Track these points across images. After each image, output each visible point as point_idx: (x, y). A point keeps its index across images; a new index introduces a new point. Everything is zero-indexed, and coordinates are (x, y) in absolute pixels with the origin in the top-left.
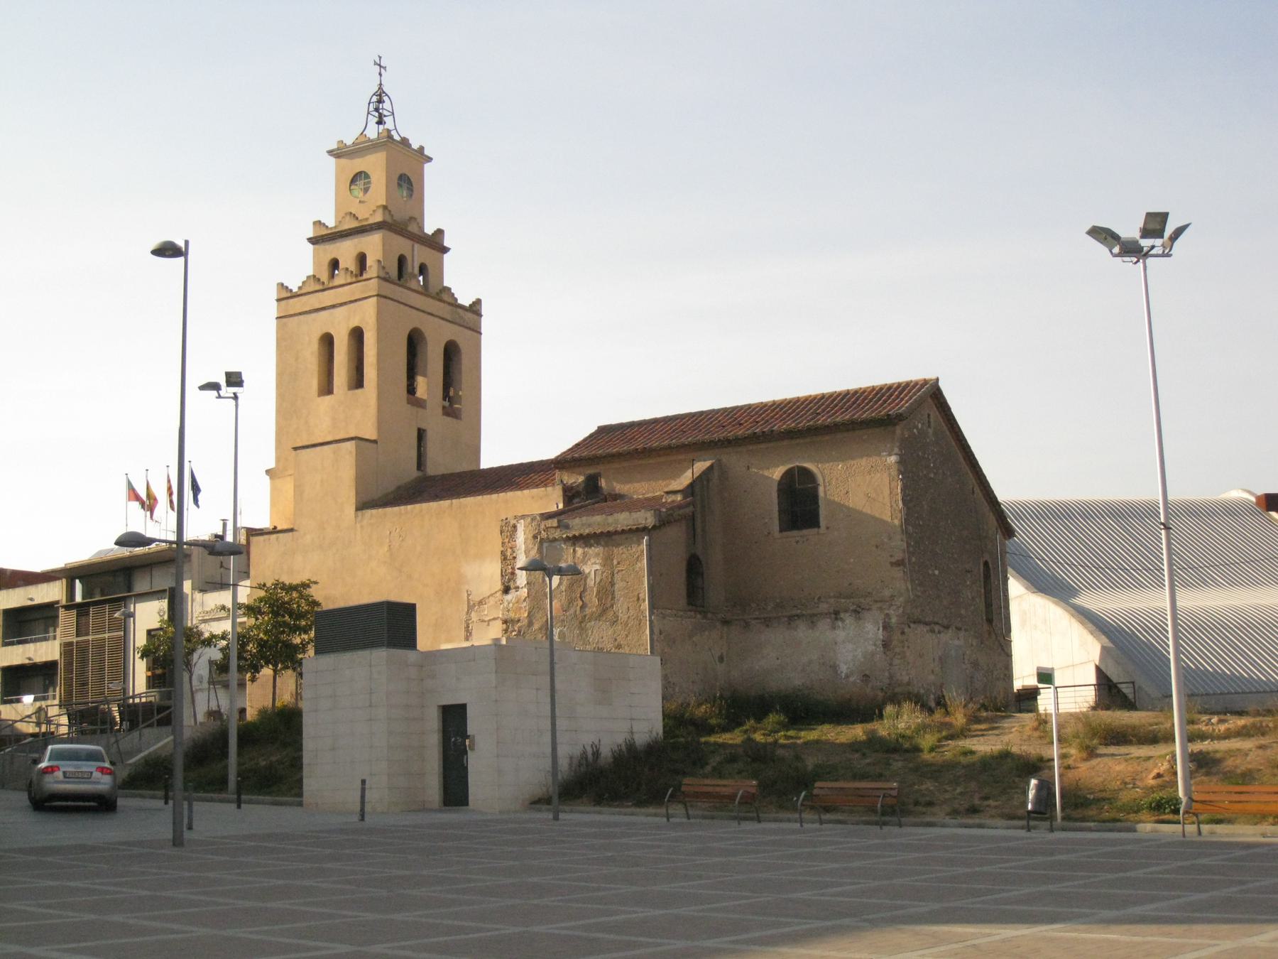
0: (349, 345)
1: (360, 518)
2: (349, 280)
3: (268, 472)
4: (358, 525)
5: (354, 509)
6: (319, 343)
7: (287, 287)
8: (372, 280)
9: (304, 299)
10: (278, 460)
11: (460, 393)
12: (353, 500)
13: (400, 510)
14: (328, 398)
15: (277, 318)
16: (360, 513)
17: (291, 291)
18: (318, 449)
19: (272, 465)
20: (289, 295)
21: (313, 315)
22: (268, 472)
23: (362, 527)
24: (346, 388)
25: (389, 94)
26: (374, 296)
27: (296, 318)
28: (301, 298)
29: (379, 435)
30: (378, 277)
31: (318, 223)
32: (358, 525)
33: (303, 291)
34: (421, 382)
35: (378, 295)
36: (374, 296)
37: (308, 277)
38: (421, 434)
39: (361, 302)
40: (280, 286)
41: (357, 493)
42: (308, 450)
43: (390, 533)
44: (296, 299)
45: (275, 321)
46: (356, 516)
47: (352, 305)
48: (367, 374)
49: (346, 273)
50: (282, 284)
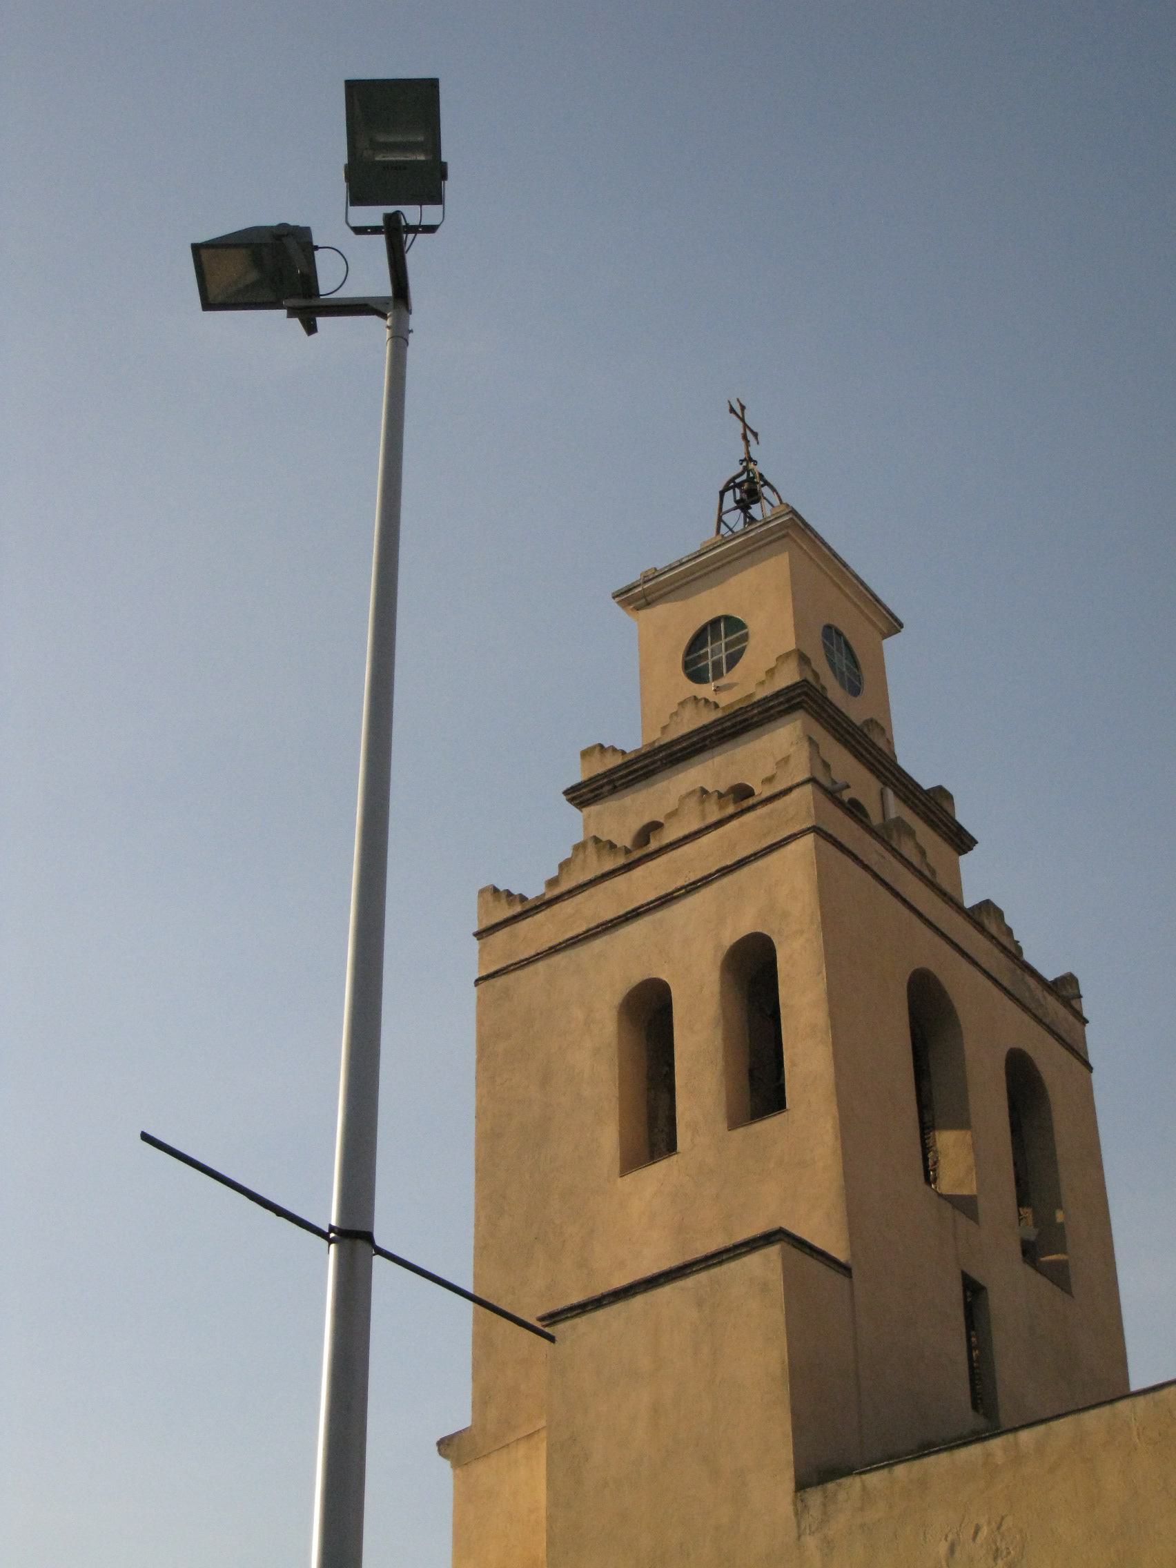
0: (723, 994)
1: (815, 1511)
2: (714, 815)
3: (445, 1445)
4: (811, 1542)
5: (790, 1485)
6: (620, 1021)
7: (509, 894)
8: (795, 794)
9: (567, 907)
10: (482, 1400)
11: (1060, 1216)
12: (785, 1453)
13: (988, 1455)
14: (660, 1169)
15: (478, 982)
16: (814, 1497)
17: (523, 899)
18: (638, 1301)
19: (459, 1417)
20: (518, 909)
21: (598, 944)
22: (445, 1445)
23: (828, 1545)
24: (722, 1125)
25: (772, 483)
26: (803, 833)
27: (541, 966)
28: (556, 908)
29: (853, 1255)
30: (812, 780)
31: (597, 750)
32: (811, 1542)
33: (557, 891)
34: (947, 1141)
35: (815, 830)
36: (803, 833)
37: (579, 848)
38: (973, 1291)
39: (761, 863)
40: (489, 897)
41: (798, 1429)
42: (600, 1315)
43: (952, 1550)
44: (540, 917)
45: (474, 991)
46: (800, 1509)
47: (725, 881)
48: (794, 1064)
49: (702, 802)
50: (495, 890)
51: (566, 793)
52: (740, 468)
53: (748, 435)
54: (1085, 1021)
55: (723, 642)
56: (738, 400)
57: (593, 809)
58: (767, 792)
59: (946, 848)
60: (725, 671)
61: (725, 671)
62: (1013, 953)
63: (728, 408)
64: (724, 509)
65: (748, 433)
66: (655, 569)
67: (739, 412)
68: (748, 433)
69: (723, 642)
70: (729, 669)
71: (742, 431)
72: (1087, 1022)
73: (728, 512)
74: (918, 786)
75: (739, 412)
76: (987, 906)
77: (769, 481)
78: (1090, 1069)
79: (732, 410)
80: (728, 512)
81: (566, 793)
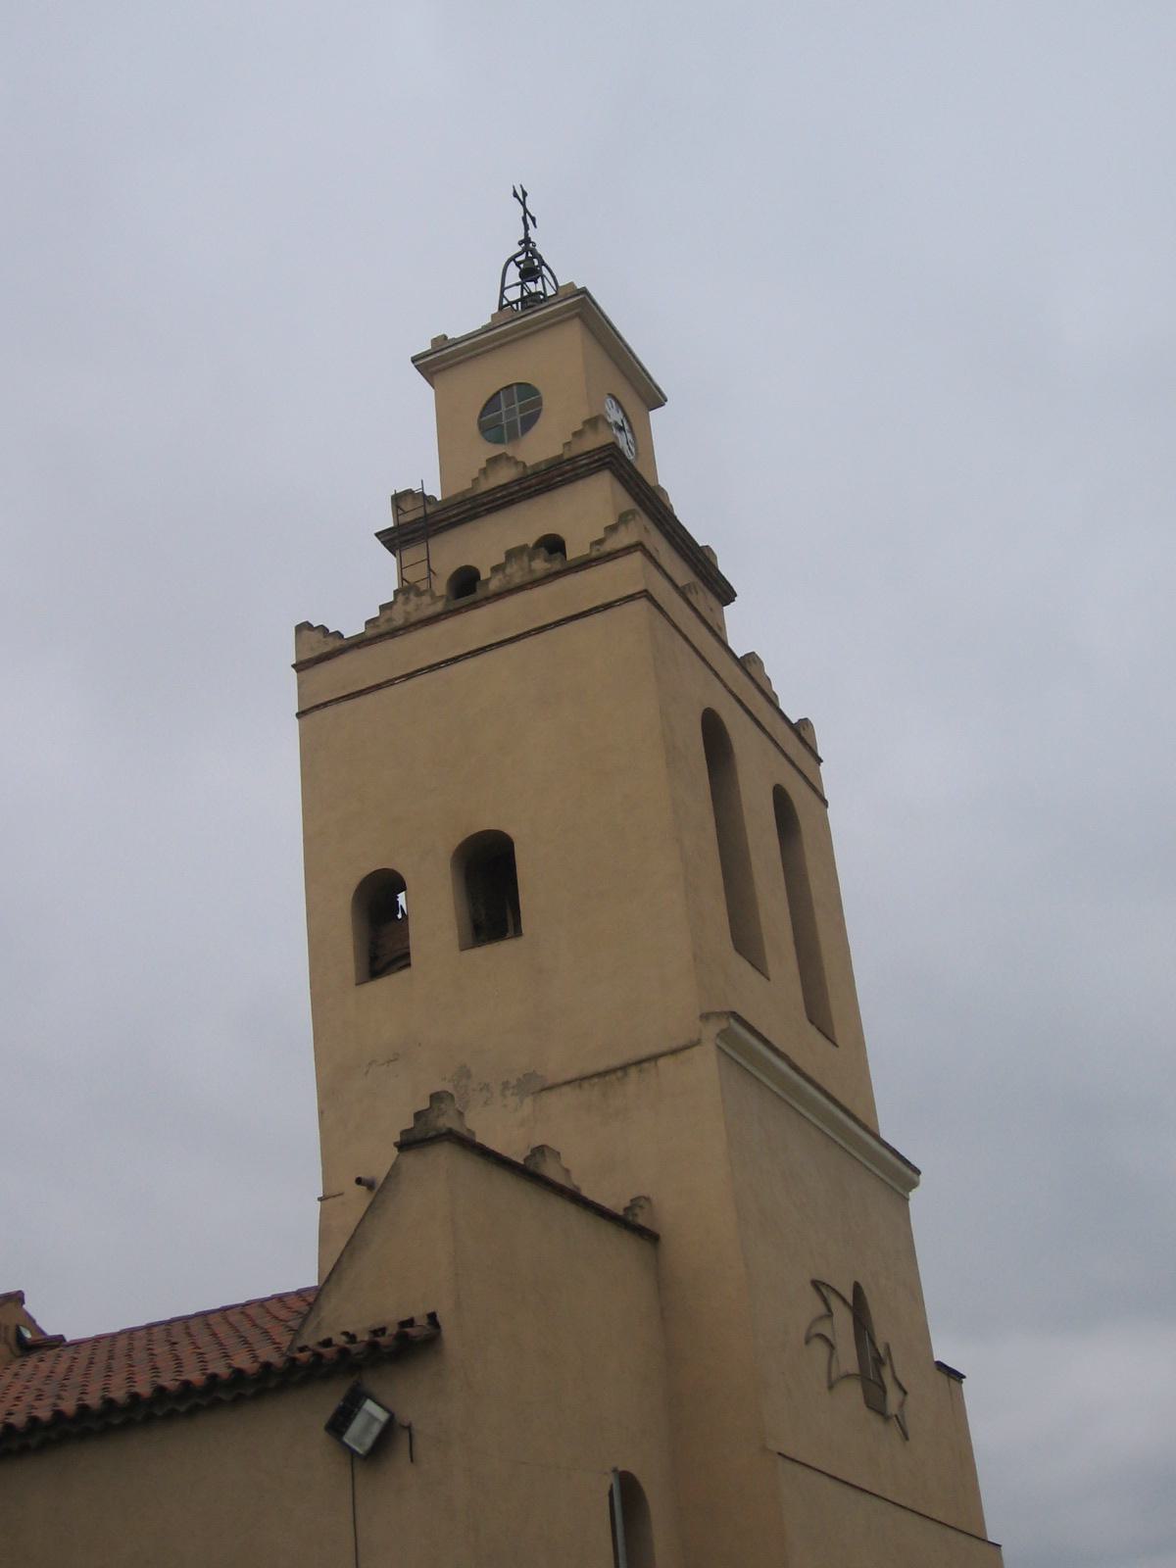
17: (338, 635)
51: (414, 360)
52: (519, 249)
53: (528, 220)
54: (819, 761)
55: (517, 405)
56: (521, 186)
57: (303, 673)
58: (495, 585)
59: (713, 601)
60: (520, 434)
61: (520, 434)
62: (771, 700)
63: (512, 191)
64: (506, 285)
65: (528, 217)
66: (445, 337)
67: (521, 197)
68: (528, 217)
69: (517, 405)
70: (523, 434)
71: (522, 214)
72: (821, 761)
73: (510, 287)
74: (697, 544)
75: (521, 197)
76: (752, 658)
77: (546, 261)
78: (825, 803)
79: (515, 195)
80: (510, 287)
81: (414, 360)
